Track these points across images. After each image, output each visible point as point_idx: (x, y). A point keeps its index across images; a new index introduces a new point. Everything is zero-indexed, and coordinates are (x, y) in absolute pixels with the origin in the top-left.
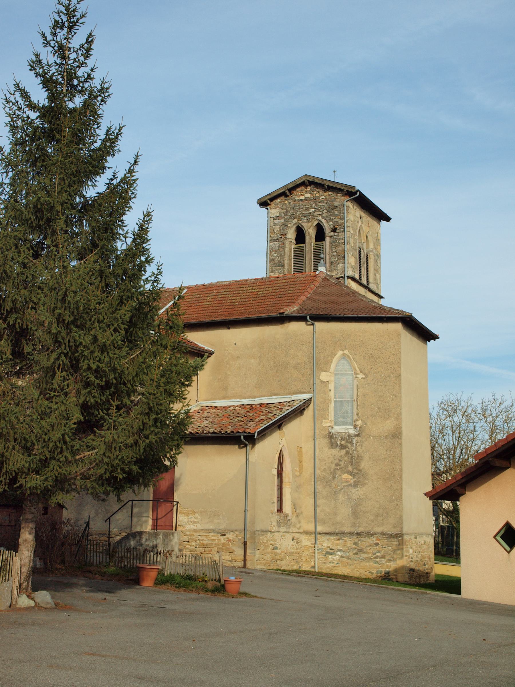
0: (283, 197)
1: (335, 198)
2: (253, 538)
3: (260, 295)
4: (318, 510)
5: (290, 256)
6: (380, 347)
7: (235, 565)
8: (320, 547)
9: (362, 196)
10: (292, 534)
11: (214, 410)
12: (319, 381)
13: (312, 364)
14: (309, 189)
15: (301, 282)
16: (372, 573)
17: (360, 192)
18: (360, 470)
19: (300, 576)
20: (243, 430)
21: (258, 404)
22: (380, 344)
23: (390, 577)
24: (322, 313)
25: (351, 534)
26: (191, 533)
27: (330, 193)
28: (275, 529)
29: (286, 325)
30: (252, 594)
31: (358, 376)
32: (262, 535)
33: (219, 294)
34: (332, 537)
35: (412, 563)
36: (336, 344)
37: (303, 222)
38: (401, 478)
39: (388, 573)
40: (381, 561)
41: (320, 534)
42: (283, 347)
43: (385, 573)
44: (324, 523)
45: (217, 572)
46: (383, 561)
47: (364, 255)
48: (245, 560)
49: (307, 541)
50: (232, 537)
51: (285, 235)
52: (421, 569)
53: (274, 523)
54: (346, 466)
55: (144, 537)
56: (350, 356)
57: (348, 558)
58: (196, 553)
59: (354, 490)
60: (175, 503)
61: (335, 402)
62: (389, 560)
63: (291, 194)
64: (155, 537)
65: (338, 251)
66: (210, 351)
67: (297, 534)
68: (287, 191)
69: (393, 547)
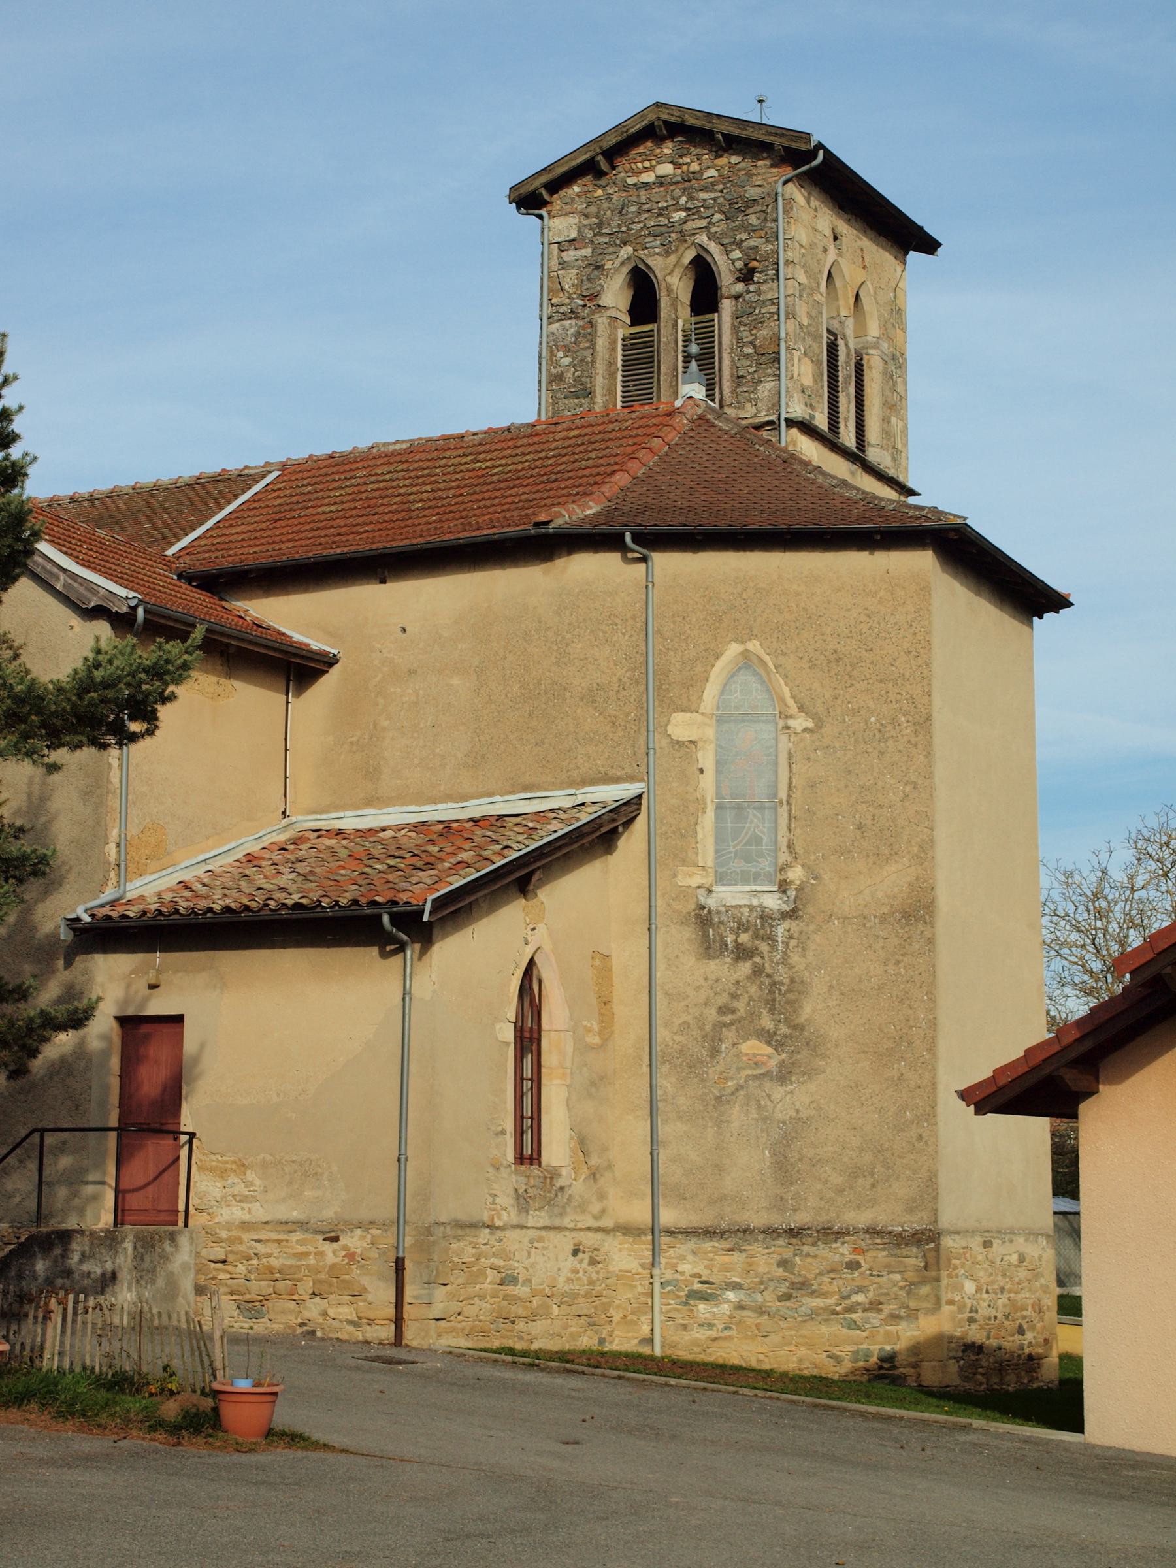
0: (590, 177)
1: (750, 175)
2: (424, 1246)
3: (495, 478)
4: (663, 1156)
5: (611, 363)
6: (865, 627)
7: (369, 1336)
8: (669, 1275)
9: (832, 161)
10: (574, 1234)
11: (332, 842)
12: (665, 742)
13: (642, 688)
14: (668, 148)
15: (626, 433)
16: (838, 1359)
17: (827, 152)
18: (800, 1028)
19: (571, 1371)
20: (390, 895)
21: (471, 820)
22: (863, 618)
23: (896, 1372)
24: (674, 522)
25: (770, 1232)
26: (234, 1233)
27: (734, 159)
28: (509, 1216)
29: (560, 563)
30: (316, 1436)
31: (791, 723)
32: (457, 1238)
33: (373, 479)
34: (708, 1245)
35: (973, 1326)
36: (720, 620)
37: (650, 255)
38: (932, 1049)
39: (889, 1359)
40: (867, 1320)
41: (670, 1233)
42: (550, 634)
43: (881, 1359)
44: (680, 1197)
45: (205, 1358)
46: (875, 1318)
47: (848, 354)
48: (399, 1321)
49: (625, 1257)
50: (359, 1244)
51: (594, 296)
52: (1007, 1345)
53: (505, 1200)
54: (753, 1015)
55: (78, 1247)
56: (767, 658)
57: (761, 1311)
58: (247, 1297)
59: (778, 1092)
60: (184, 1138)
61: (719, 808)
62: (894, 1318)
63: (614, 168)
64: (111, 1247)
65: (757, 343)
66: (326, 654)
67: (590, 1234)
68: (600, 158)
69: (907, 1275)
